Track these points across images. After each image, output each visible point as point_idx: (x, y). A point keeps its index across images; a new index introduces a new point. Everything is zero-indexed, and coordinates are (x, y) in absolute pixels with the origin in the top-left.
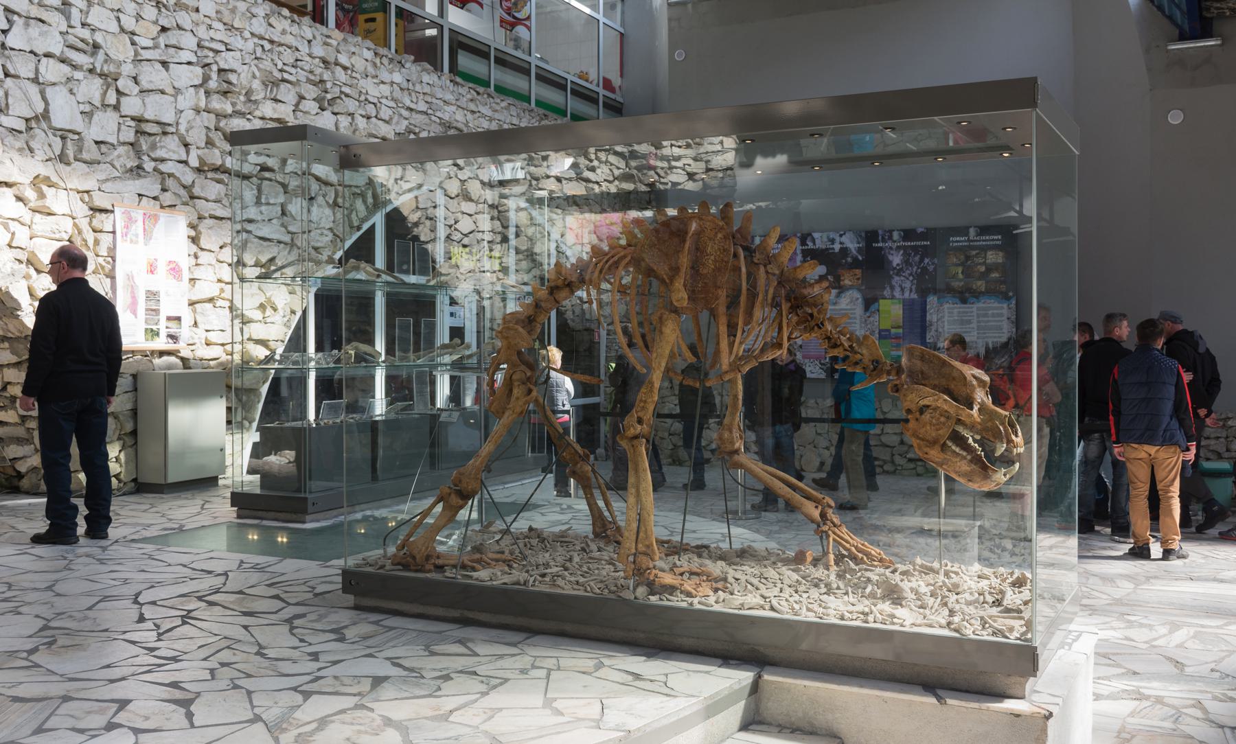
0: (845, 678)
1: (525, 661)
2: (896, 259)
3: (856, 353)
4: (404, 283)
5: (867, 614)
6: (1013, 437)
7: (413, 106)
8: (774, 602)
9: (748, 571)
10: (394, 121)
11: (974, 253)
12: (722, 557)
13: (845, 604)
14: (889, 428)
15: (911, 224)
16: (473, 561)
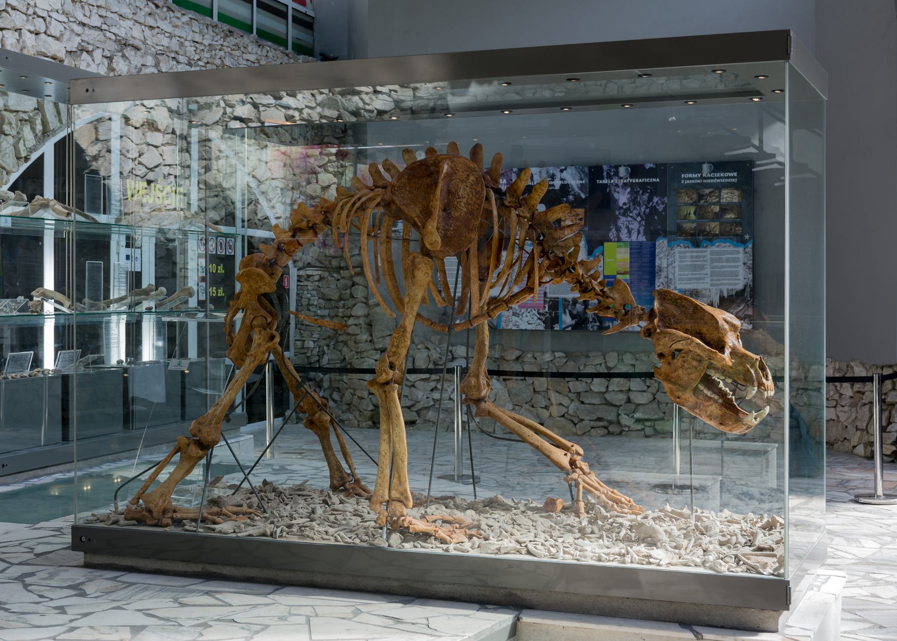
0: (603, 618)
1: (280, 610)
2: (622, 198)
3: (608, 297)
4: (96, 223)
5: (624, 555)
6: (764, 380)
7: (86, 20)
8: (531, 546)
9: (499, 517)
10: (65, 37)
11: (707, 191)
12: (471, 506)
13: (601, 547)
14: (616, 384)
15: (638, 156)
16: (212, 514)
